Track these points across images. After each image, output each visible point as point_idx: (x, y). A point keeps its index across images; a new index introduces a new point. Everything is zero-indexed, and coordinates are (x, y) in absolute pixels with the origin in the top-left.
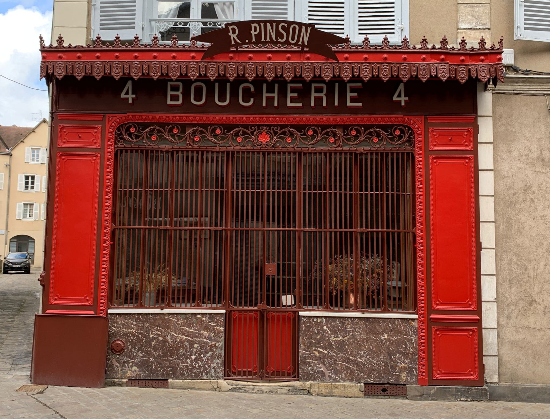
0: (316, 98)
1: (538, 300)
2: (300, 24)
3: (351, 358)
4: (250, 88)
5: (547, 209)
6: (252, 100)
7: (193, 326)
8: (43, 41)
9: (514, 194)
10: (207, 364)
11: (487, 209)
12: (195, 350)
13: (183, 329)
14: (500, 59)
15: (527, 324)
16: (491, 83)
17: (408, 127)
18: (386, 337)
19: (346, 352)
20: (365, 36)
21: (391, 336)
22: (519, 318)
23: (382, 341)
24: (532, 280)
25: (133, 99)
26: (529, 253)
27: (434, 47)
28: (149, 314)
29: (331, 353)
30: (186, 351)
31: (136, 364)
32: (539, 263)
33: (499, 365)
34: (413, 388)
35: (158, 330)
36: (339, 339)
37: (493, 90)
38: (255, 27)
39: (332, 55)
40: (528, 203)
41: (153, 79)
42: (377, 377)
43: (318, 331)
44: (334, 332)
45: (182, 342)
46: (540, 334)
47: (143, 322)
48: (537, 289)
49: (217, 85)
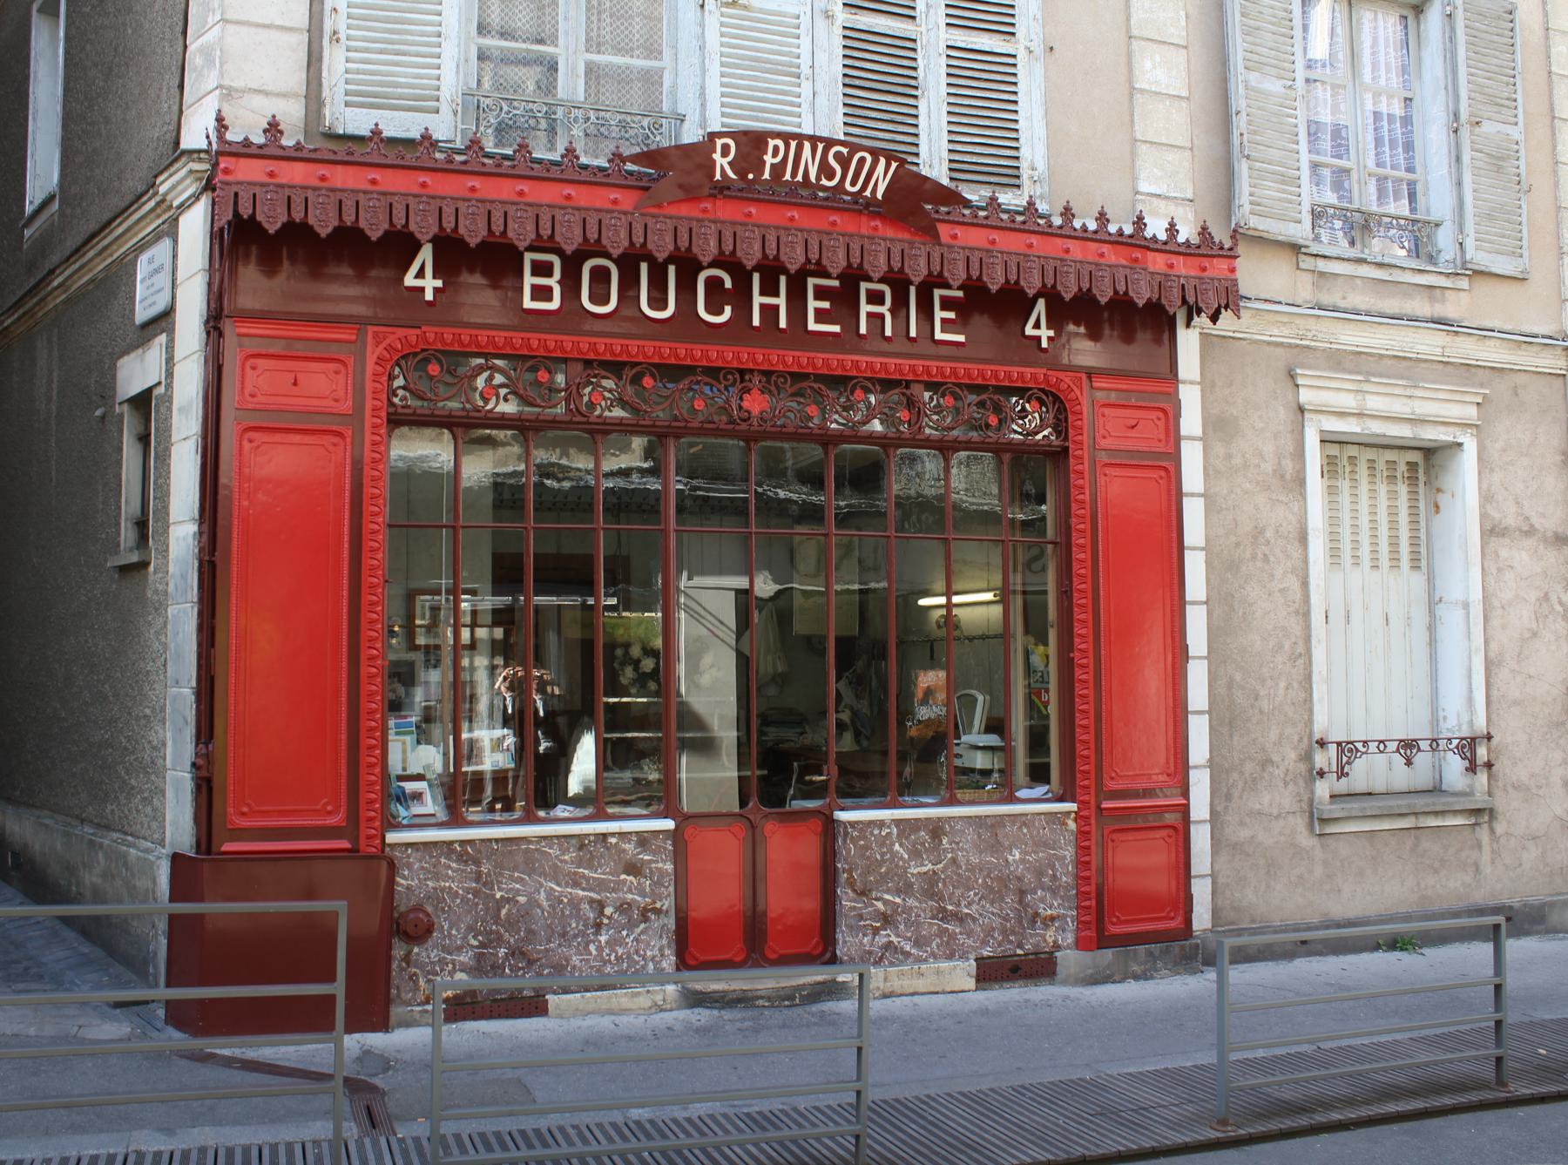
0: (763, 307)
1: (1276, 758)
4: (722, 281)
6: (728, 309)
7: (600, 865)
8: (226, 128)
9: (1237, 545)
10: (637, 952)
12: (606, 921)
13: (575, 873)
15: (1258, 806)
17: (1053, 394)
21: (1026, 853)
25: (436, 290)
27: (1120, 233)
28: (490, 840)
30: (586, 926)
33: (1214, 893)
35: (512, 878)
36: (925, 869)
40: (1259, 564)
43: (882, 855)
44: (915, 854)
45: (575, 903)
48: (1273, 736)
49: (672, 269)
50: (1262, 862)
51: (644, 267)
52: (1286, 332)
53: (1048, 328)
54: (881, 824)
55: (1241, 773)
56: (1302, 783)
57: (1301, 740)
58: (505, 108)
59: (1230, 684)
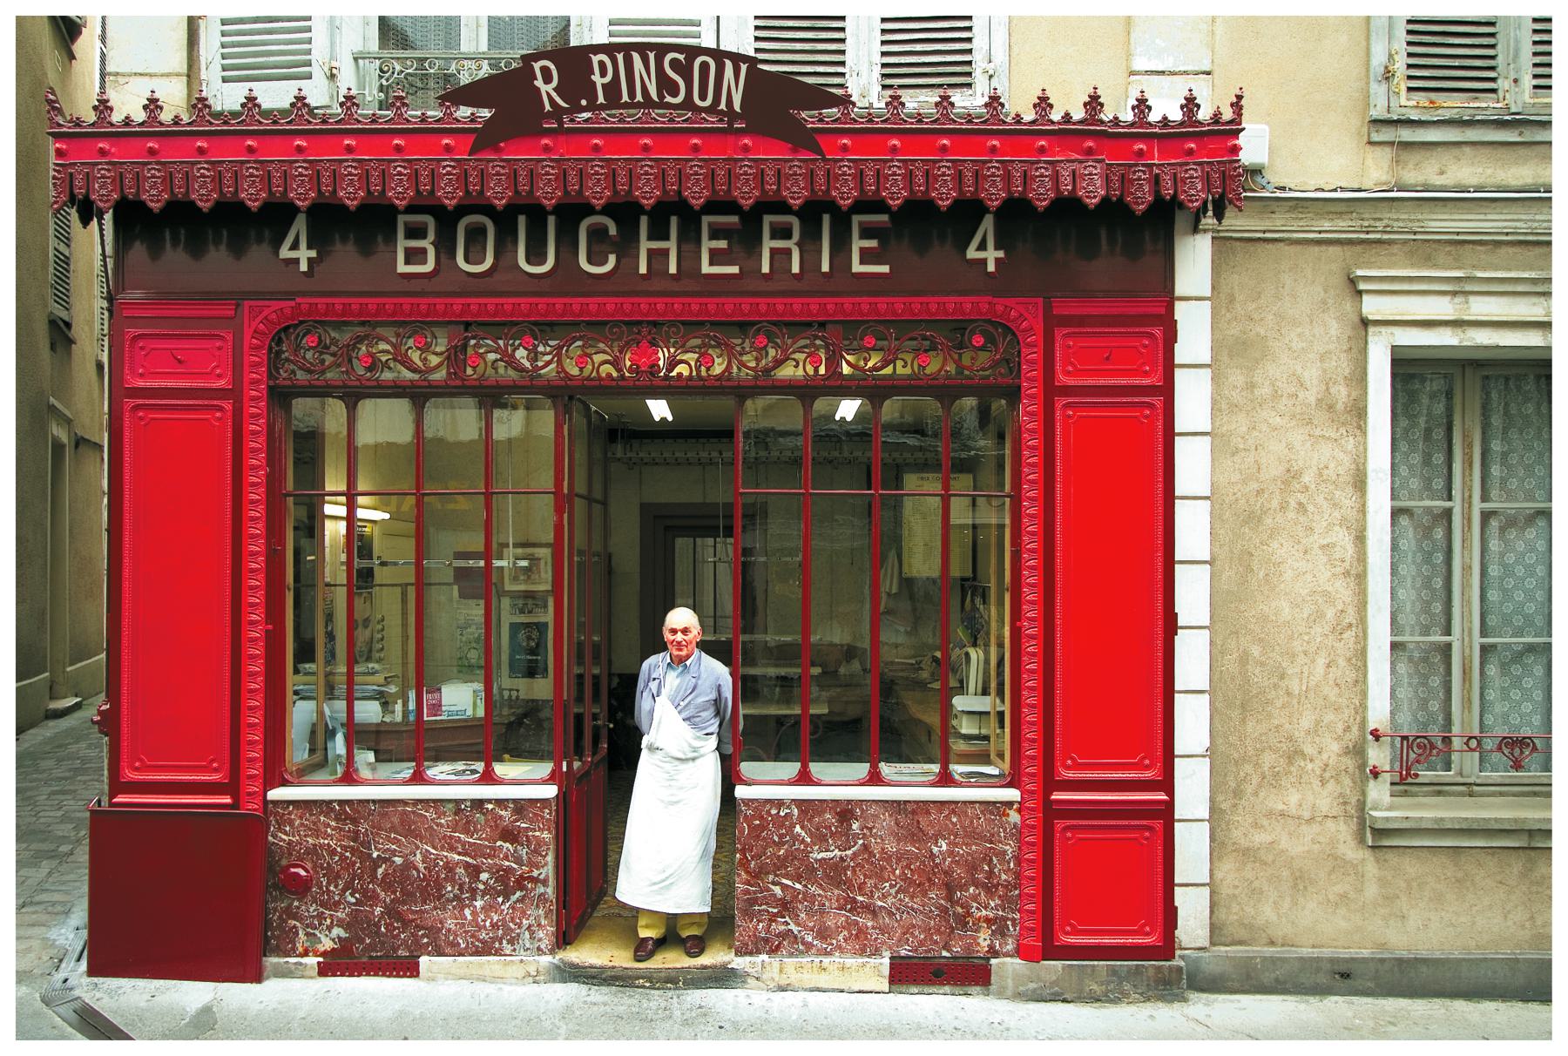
1: (1309, 749)
2: (719, 55)
3: (860, 898)
4: (606, 230)
5: (1337, 528)
6: (612, 259)
7: (476, 831)
9: (1259, 492)
10: (512, 920)
11: (1192, 531)
14: (1236, 150)
15: (1281, 807)
16: (1210, 213)
18: (944, 847)
19: (849, 885)
20: (941, 92)
21: (956, 845)
22: (1262, 794)
23: (932, 856)
24: (1295, 701)
26: (1291, 638)
27: (1067, 117)
29: (813, 889)
30: (461, 889)
31: (341, 923)
32: (1313, 661)
34: (1008, 967)
37: (1214, 231)
38: (602, 64)
39: (805, 140)
40: (1291, 515)
41: (345, 207)
42: (921, 944)
43: (781, 836)
44: (820, 839)
45: (450, 868)
46: (1309, 832)
47: (355, 821)
48: (1306, 722)
50: (1285, 873)
51: (826, 219)
52: (1342, 224)
53: (996, 249)
54: (779, 803)
55: (1257, 765)
56: (1347, 781)
57: (1347, 729)
58: (398, 68)
59: (1244, 659)
